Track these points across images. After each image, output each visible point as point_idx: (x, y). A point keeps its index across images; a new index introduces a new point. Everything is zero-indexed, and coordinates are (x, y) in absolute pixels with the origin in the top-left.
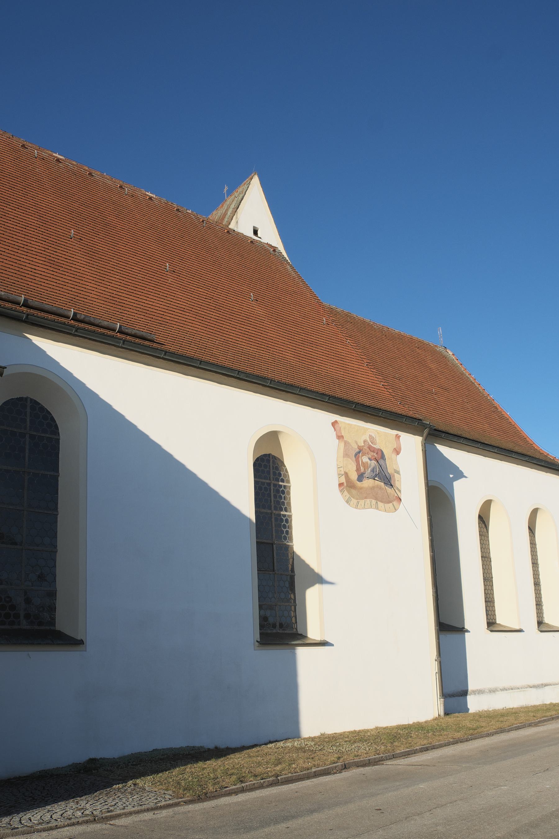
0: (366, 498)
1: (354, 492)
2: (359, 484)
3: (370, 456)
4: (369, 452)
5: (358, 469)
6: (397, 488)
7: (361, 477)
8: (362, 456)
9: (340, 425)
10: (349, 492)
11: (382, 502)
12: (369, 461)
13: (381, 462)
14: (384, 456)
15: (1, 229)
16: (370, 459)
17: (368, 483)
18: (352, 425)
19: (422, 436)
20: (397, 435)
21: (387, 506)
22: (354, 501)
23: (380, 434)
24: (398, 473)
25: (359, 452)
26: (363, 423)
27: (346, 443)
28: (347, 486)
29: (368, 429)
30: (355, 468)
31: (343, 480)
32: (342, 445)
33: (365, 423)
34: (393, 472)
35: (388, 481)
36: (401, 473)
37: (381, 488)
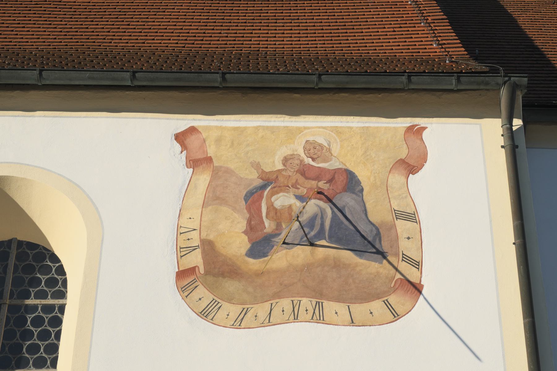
0: (278, 295)
1: (231, 286)
2: (254, 264)
3: (303, 191)
4: (301, 179)
5: (252, 227)
6: (406, 259)
7: (260, 247)
8: (273, 194)
9: (204, 135)
10: (210, 288)
11: (338, 299)
12: (298, 204)
13: (347, 200)
14: (358, 182)
15: (556, 85)
16: (300, 198)
17: (281, 259)
18: (245, 128)
19: (499, 117)
20: (410, 129)
21: (359, 310)
22: (231, 310)
23: (348, 137)
24: (412, 217)
25: (263, 187)
26: (287, 118)
27: (216, 173)
28: (207, 273)
29: (300, 130)
30: (242, 225)
31: (196, 259)
32: (204, 179)
33: (294, 118)
34: (389, 218)
35: (370, 243)
36: (422, 216)
37: (337, 265)
